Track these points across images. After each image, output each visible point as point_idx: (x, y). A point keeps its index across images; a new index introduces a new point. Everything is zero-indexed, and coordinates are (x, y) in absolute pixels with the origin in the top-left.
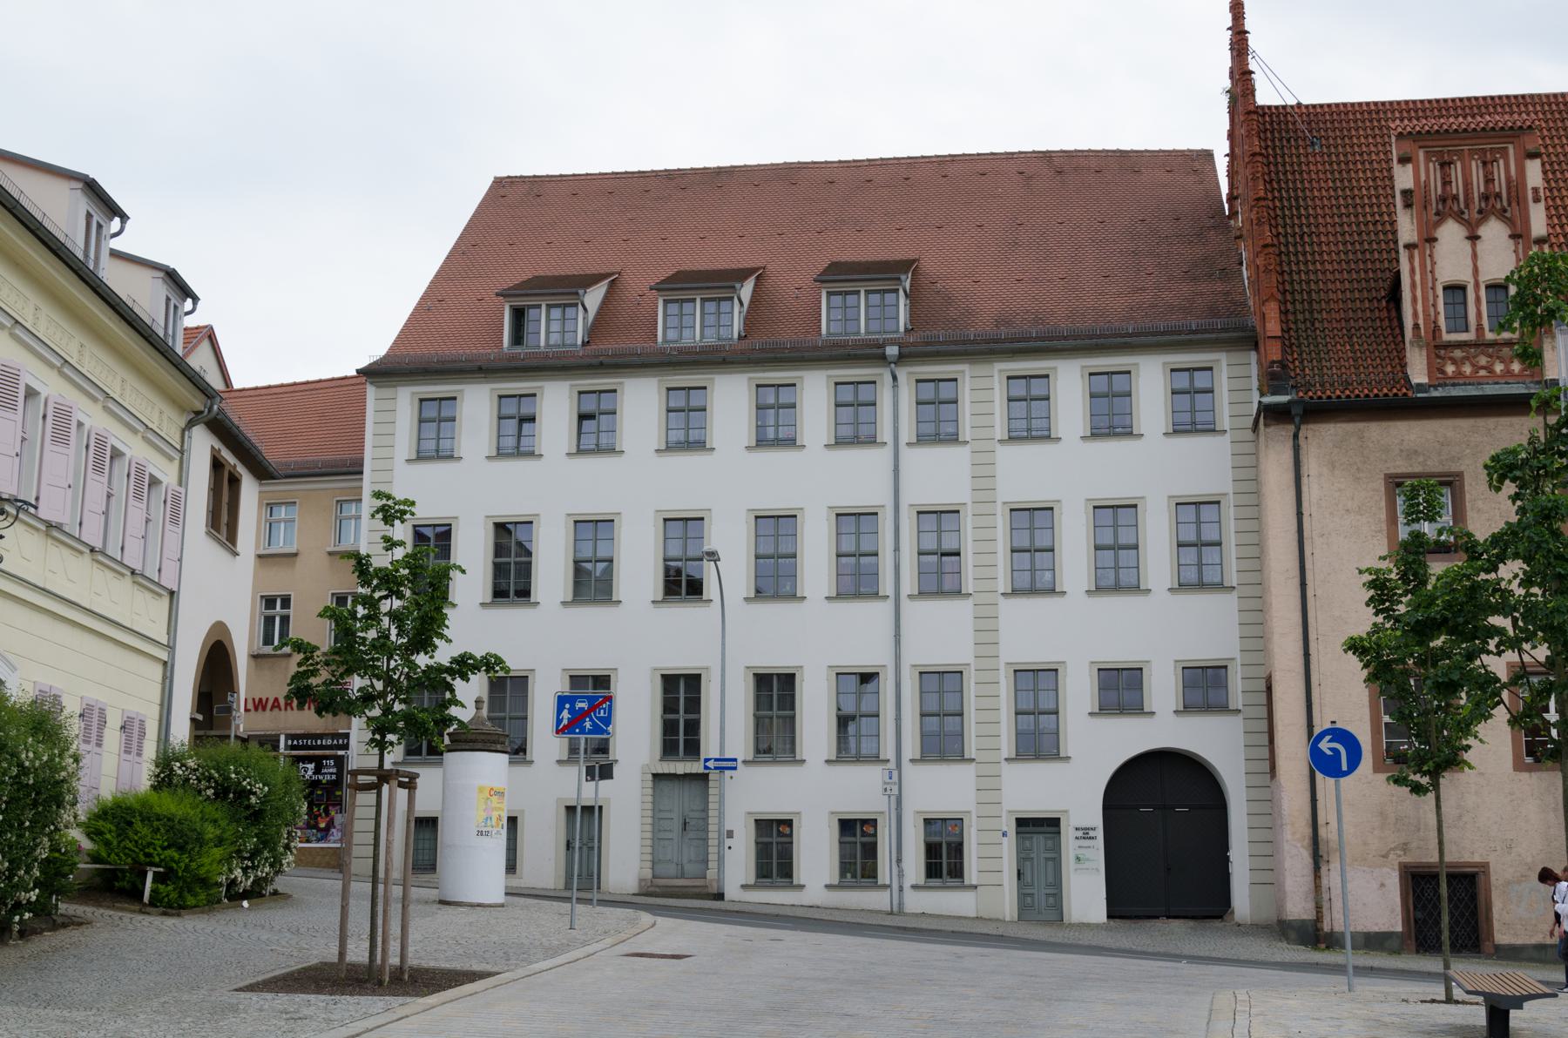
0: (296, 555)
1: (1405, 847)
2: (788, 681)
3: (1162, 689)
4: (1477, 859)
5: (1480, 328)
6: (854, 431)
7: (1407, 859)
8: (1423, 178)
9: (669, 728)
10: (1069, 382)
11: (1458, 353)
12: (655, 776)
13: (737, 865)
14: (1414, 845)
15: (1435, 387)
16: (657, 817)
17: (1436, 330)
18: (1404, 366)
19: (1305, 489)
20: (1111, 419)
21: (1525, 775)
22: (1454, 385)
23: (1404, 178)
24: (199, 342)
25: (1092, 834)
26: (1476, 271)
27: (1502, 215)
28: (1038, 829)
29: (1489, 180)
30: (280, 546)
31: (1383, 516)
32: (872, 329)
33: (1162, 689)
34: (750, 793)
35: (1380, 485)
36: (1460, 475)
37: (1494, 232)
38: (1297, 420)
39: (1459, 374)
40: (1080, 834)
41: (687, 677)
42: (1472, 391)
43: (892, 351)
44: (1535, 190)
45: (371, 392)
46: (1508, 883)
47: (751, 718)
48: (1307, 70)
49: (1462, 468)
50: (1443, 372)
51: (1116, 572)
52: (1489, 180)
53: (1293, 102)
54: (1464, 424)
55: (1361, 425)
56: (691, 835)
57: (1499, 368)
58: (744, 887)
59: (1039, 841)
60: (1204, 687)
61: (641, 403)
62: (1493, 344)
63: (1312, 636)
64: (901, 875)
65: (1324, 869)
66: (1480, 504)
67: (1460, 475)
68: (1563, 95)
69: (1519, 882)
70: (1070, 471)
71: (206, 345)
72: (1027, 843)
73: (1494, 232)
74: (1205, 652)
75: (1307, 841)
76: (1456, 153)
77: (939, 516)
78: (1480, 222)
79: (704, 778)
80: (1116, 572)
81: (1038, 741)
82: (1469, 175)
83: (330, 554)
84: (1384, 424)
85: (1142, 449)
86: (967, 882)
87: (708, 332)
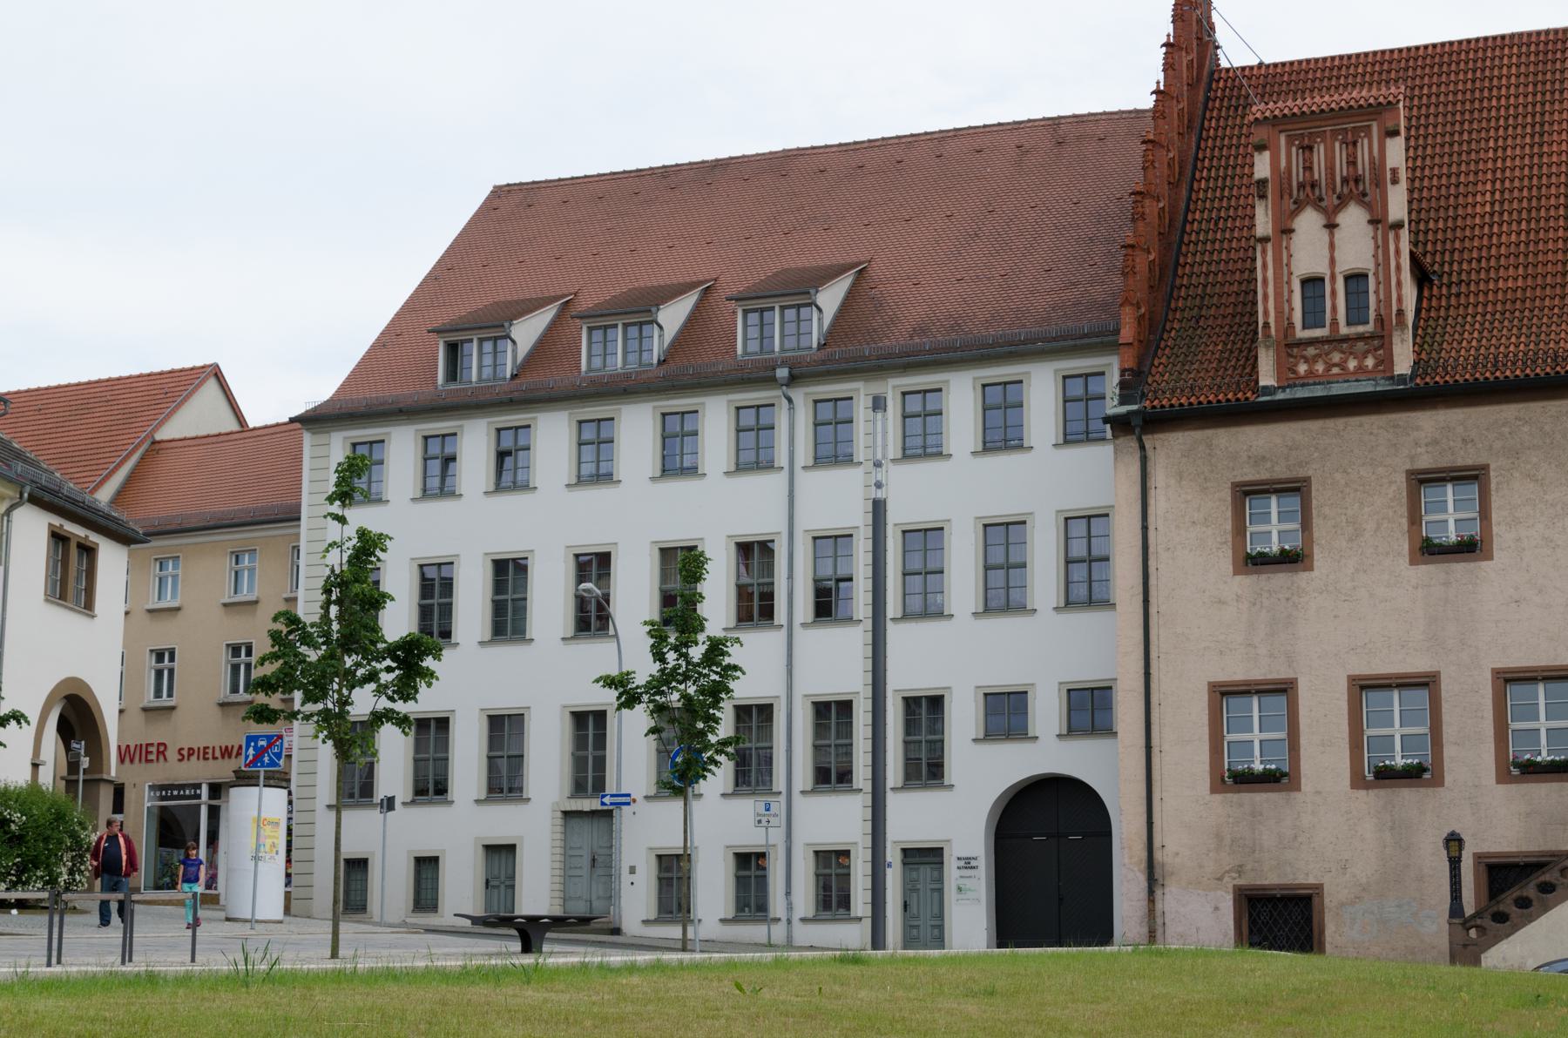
0: (256, 602)
1: (1240, 870)
2: (936, 703)
3: (1047, 713)
4: (1311, 880)
5: (1335, 322)
6: (753, 457)
7: (1242, 882)
8: (1283, 164)
9: (579, 763)
10: (961, 395)
11: (1311, 351)
12: (566, 814)
13: (636, 900)
14: (1249, 867)
15: (1283, 388)
16: (567, 855)
17: (1291, 325)
18: (1255, 366)
19: (1151, 501)
20: (1002, 432)
21: (1362, 793)
22: (1303, 385)
23: (1262, 167)
24: (204, 381)
25: (973, 863)
26: (1332, 261)
27: (1362, 198)
28: (925, 858)
29: (1352, 163)
30: (244, 595)
31: (1229, 526)
32: (750, 350)
33: (1047, 713)
34: (649, 828)
35: (1227, 494)
36: (1307, 480)
37: (1353, 219)
38: (1137, 431)
39: (1310, 373)
40: (962, 863)
41: (838, 703)
42: (1319, 392)
43: (782, 373)
44: (1394, 171)
45: (307, 439)
46: (1342, 905)
47: (485, 761)
48: (1250, 34)
49: (1310, 473)
50: (1295, 372)
51: (1003, 593)
52: (1352, 163)
53: (1255, 62)
54: (1314, 426)
55: (1209, 432)
56: (600, 871)
57: (1352, 364)
58: (723, 921)
59: (925, 872)
60: (1089, 709)
61: (552, 437)
62: (1346, 339)
63: (1153, 655)
64: (790, 907)
65: (1158, 892)
66: (1326, 510)
67: (1307, 480)
68: (1565, 30)
69: (1352, 903)
70: (955, 490)
71: (212, 384)
72: (914, 875)
73: (1353, 219)
74: (1088, 673)
75: (1144, 865)
76: (1318, 134)
77: (833, 542)
78: (1338, 209)
79: (608, 814)
80: (1003, 593)
81: (927, 768)
82: (1328, 158)
83: (225, 605)
84: (1233, 430)
85: (1005, 468)
86: (772, 915)
87: (631, 357)
